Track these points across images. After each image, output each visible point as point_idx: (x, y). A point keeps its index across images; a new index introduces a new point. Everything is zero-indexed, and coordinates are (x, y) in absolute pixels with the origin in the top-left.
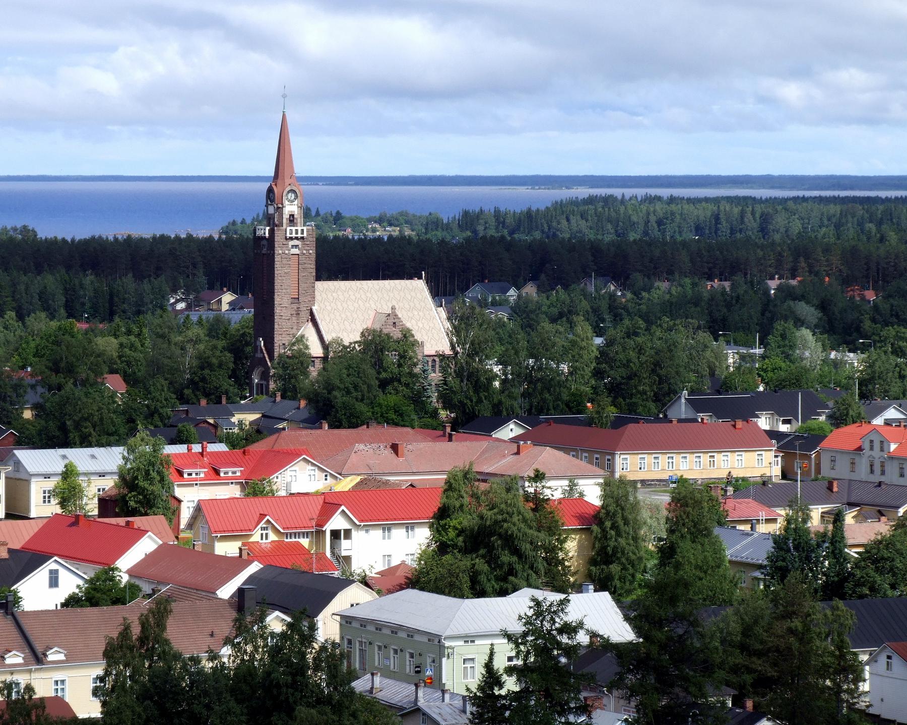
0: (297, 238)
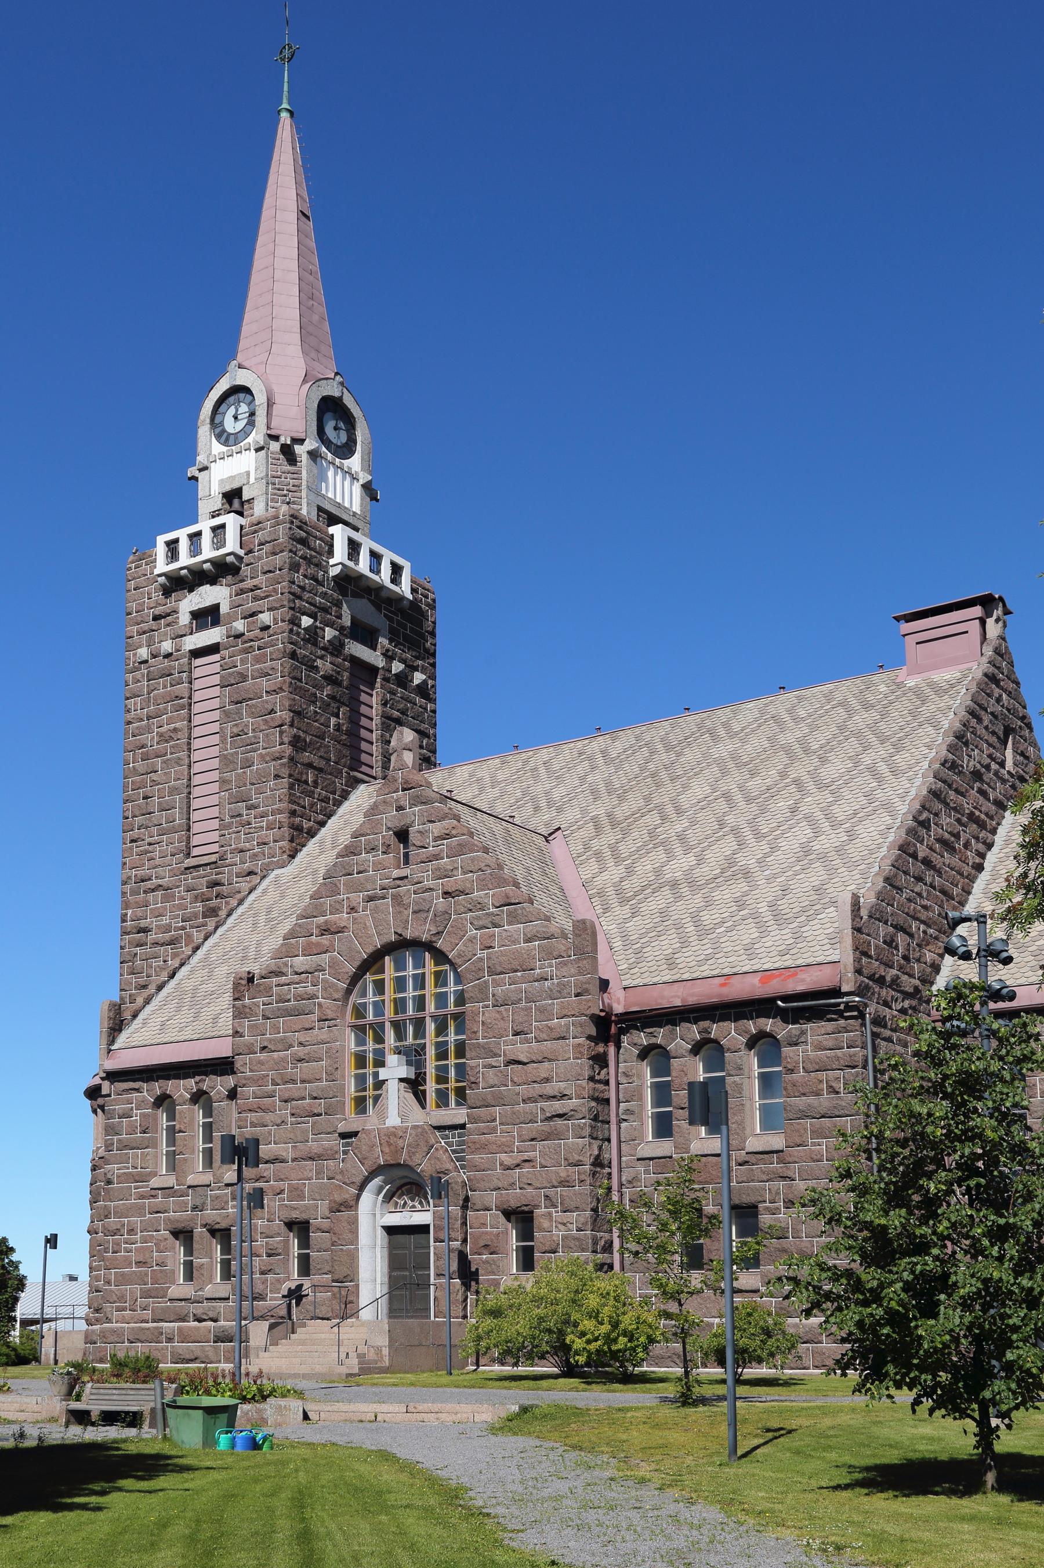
0: (197, 578)
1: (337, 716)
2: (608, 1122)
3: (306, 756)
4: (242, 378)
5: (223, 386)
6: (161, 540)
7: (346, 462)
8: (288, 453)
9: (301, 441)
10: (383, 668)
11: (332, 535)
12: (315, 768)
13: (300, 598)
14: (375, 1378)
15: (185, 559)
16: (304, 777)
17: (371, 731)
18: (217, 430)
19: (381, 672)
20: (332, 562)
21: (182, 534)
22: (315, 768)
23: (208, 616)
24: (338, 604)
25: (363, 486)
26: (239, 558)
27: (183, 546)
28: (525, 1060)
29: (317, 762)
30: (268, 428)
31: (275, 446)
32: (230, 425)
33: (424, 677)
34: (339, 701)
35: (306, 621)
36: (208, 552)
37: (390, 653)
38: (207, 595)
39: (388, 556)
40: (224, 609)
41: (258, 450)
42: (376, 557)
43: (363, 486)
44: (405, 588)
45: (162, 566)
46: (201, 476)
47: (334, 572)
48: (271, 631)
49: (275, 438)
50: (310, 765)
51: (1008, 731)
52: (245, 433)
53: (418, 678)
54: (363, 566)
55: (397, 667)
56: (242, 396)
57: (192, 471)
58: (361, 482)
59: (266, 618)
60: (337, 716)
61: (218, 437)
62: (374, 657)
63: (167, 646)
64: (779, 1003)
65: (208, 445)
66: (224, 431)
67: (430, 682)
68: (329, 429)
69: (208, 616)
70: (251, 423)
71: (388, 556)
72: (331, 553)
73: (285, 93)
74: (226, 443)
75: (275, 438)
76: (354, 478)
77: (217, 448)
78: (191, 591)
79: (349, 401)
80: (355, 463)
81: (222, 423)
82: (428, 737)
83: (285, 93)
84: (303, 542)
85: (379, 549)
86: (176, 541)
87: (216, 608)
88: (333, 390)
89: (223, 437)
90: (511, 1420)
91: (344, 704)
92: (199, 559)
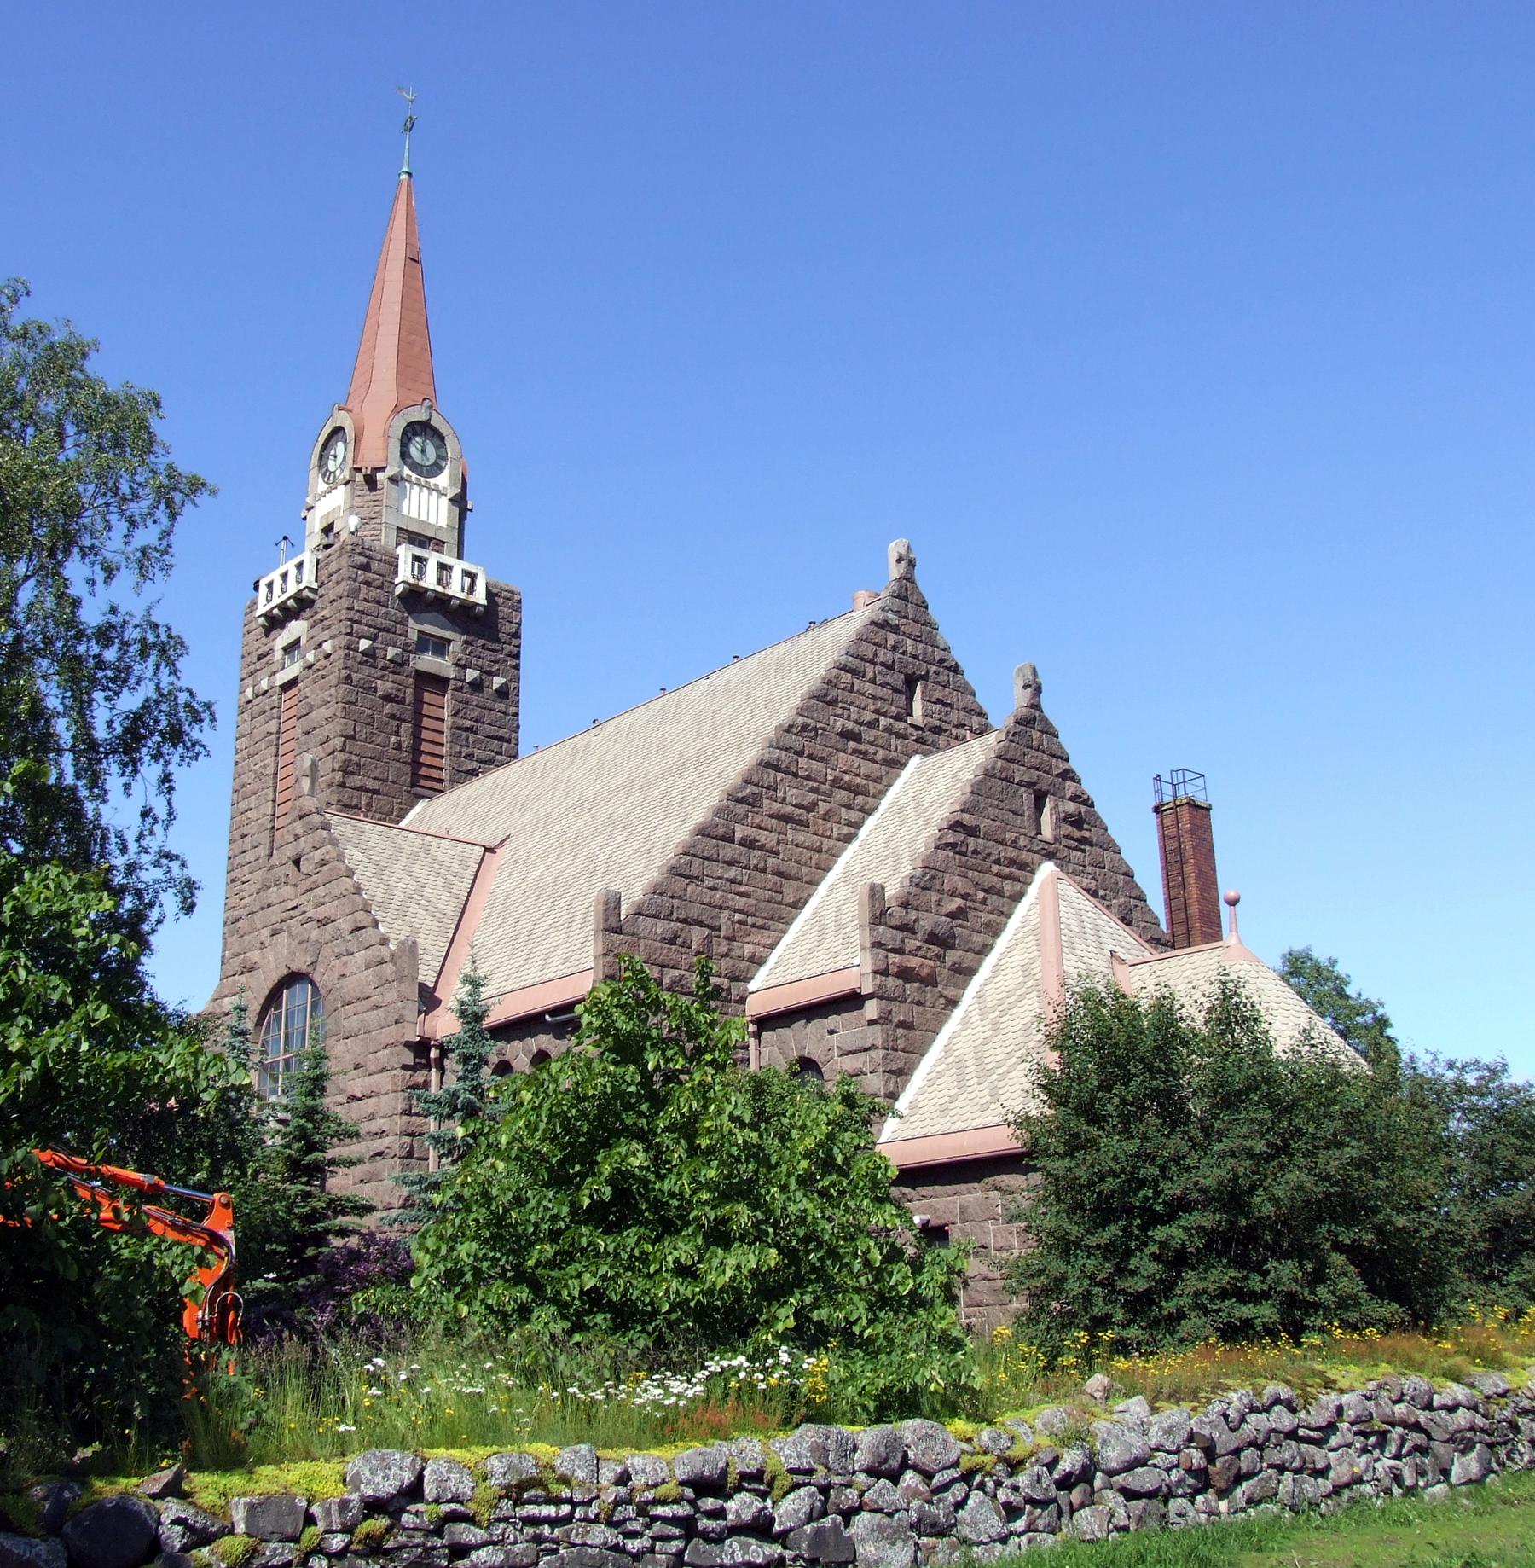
1: (397, 734)
2: (427, 1159)
3: (355, 781)
5: (328, 430)
7: (432, 481)
8: (371, 482)
9: (383, 469)
10: (455, 678)
12: (367, 790)
13: (359, 622)
16: (355, 801)
17: (442, 745)
19: (452, 682)
22: (367, 790)
24: (403, 622)
25: (450, 500)
26: (314, 591)
28: (359, 1095)
29: (371, 784)
30: (354, 462)
31: (359, 477)
33: (503, 680)
34: (399, 719)
35: (364, 644)
37: (463, 662)
38: (296, 629)
41: (346, 484)
43: (450, 500)
44: (480, 597)
47: (399, 590)
48: (331, 658)
49: (359, 470)
50: (361, 789)
51: (911, 682)
53: (498, 681)
54: (430, 581)
55: (471, 674)
58: (449, 496)
59: (327, 647)
60: (397, 734)
62: (442, 665)
63: (264, 685)
64: (547, 1017)
67: (513, 685)
68: (414, 451)
72: (396, 573)
75: (359, 470)
76: (441, 493)
77: (322, 486)
78: (282, 627)
79: (436, 421)
82: (509, 742)
84: (366, 568)
91: (404, 721)
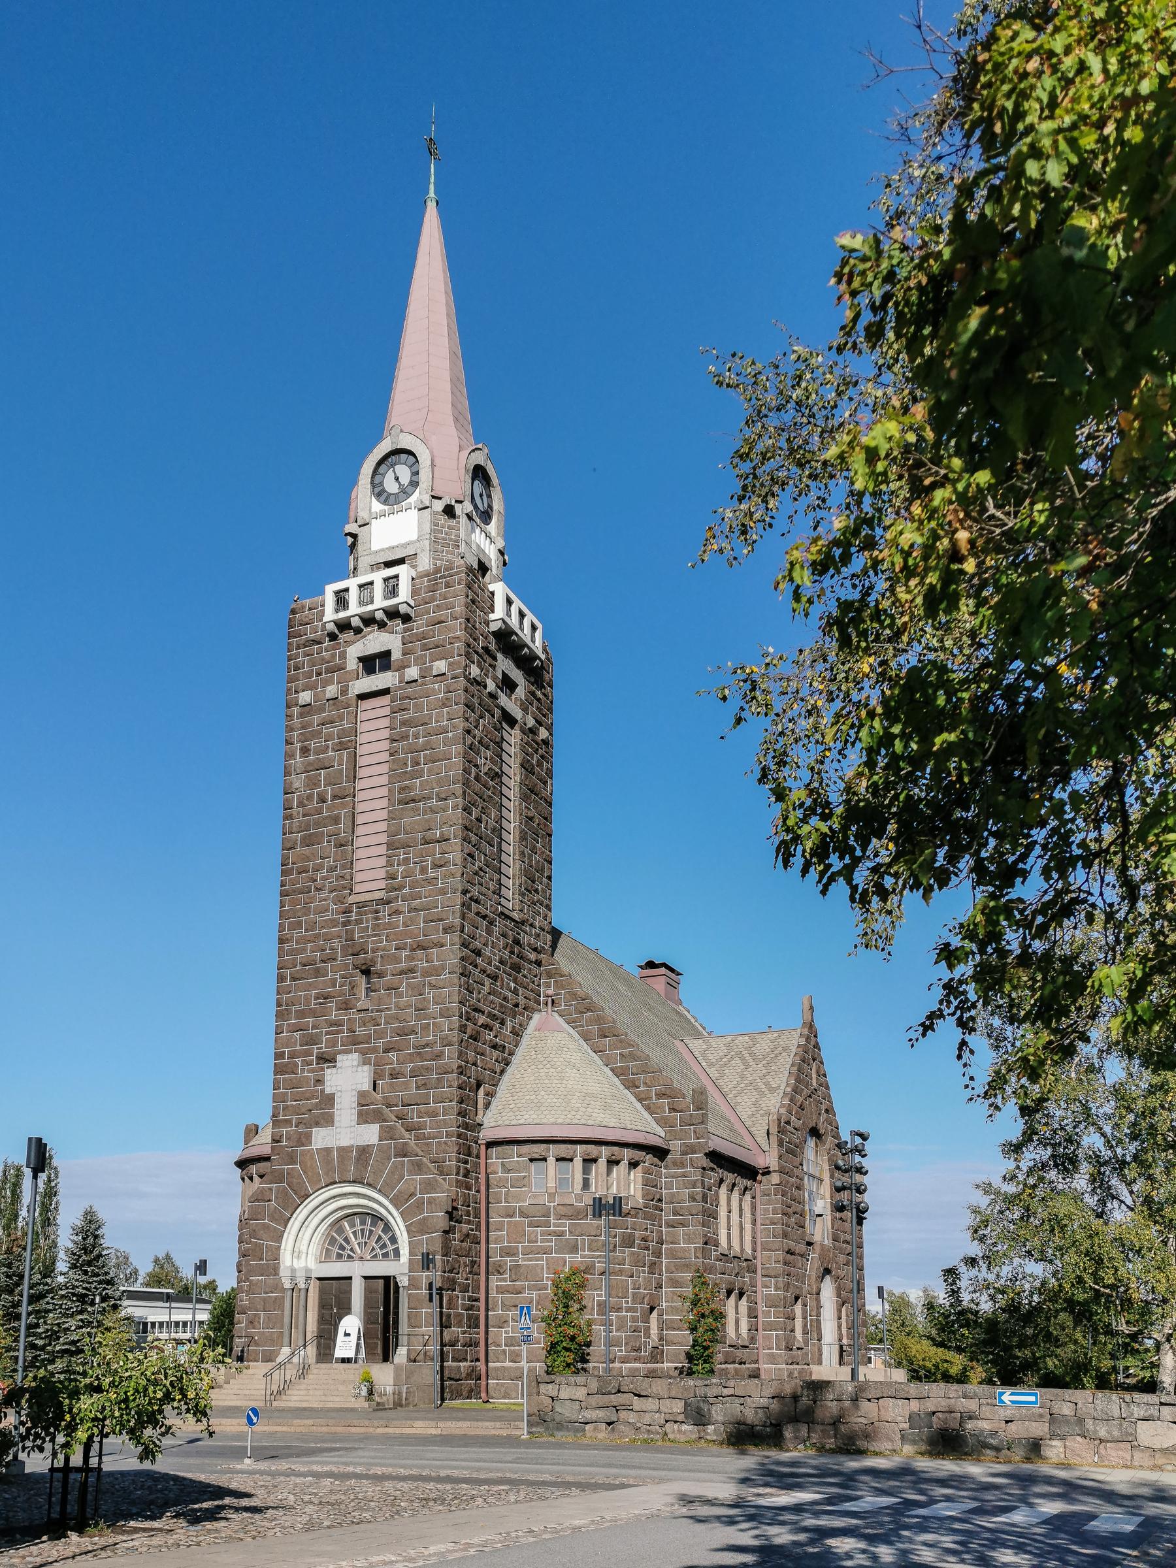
4: (405, 442)
6: (330, 589)
8: (449, 511)
11: (493, 593)
14: (510, 1471)
15: (354, 608)
18: (377, 490)
20: (492, 617)
21: (352, 583)
23: (370, 664)
27: (353, 597)
32: (391, 486)
36: (380, 602)
38: (375, 642)
39: (530, 618)
40: (396, 656)
42: (522, 615)
45: (330, 614)
46: (361, 532)
47: (494, 627)
52: (405, 493)
54: (514, 621)
56: (403, 456)
57: (351, 528)
61: (378, 496)
65: (365, 501)
66: (384, 491)
69: (374, 663)
70: (414, 484)
71: (530, 618)
72: (492, 609)
73: (432, 179)
74: (385, 502)
77: (377, 506)
80: (492, 528)
81: (381, 484)
83: (432, 179)
85: (525, 610)
86: (347, 590)
87: (387, 654)
88: (479, 458)
89: (380, 493)
90: (881, 1295)
92: (370, 608)
